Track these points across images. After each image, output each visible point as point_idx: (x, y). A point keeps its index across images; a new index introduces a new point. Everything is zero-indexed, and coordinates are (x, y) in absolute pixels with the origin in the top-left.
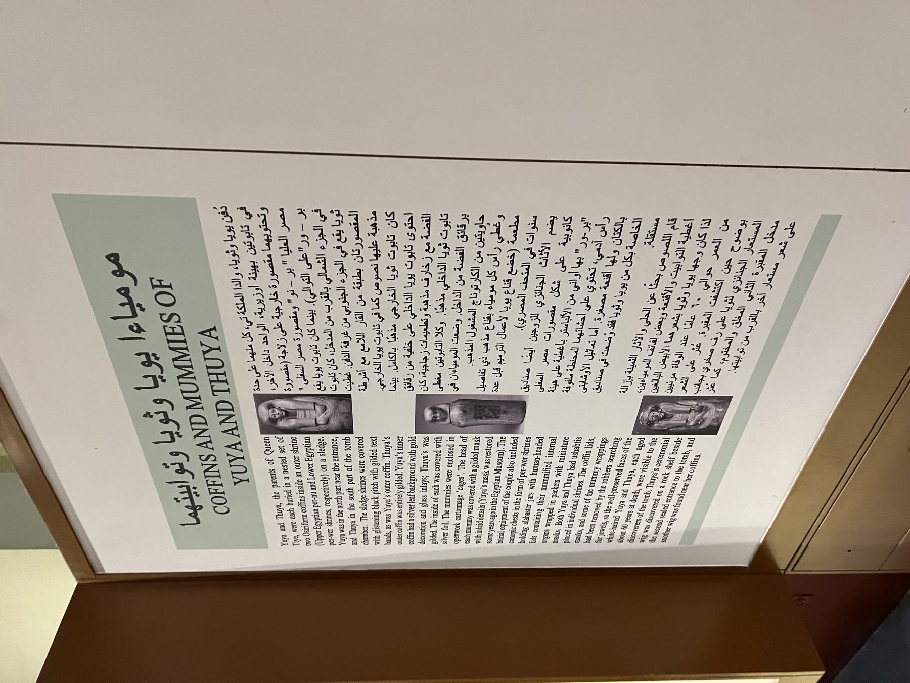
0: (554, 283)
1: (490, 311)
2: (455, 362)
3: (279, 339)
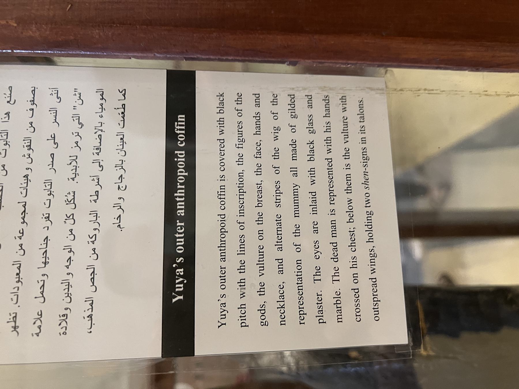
0: (69, 193)
1: (101, 120)
2: (102, 105)
3: (96, 245)
